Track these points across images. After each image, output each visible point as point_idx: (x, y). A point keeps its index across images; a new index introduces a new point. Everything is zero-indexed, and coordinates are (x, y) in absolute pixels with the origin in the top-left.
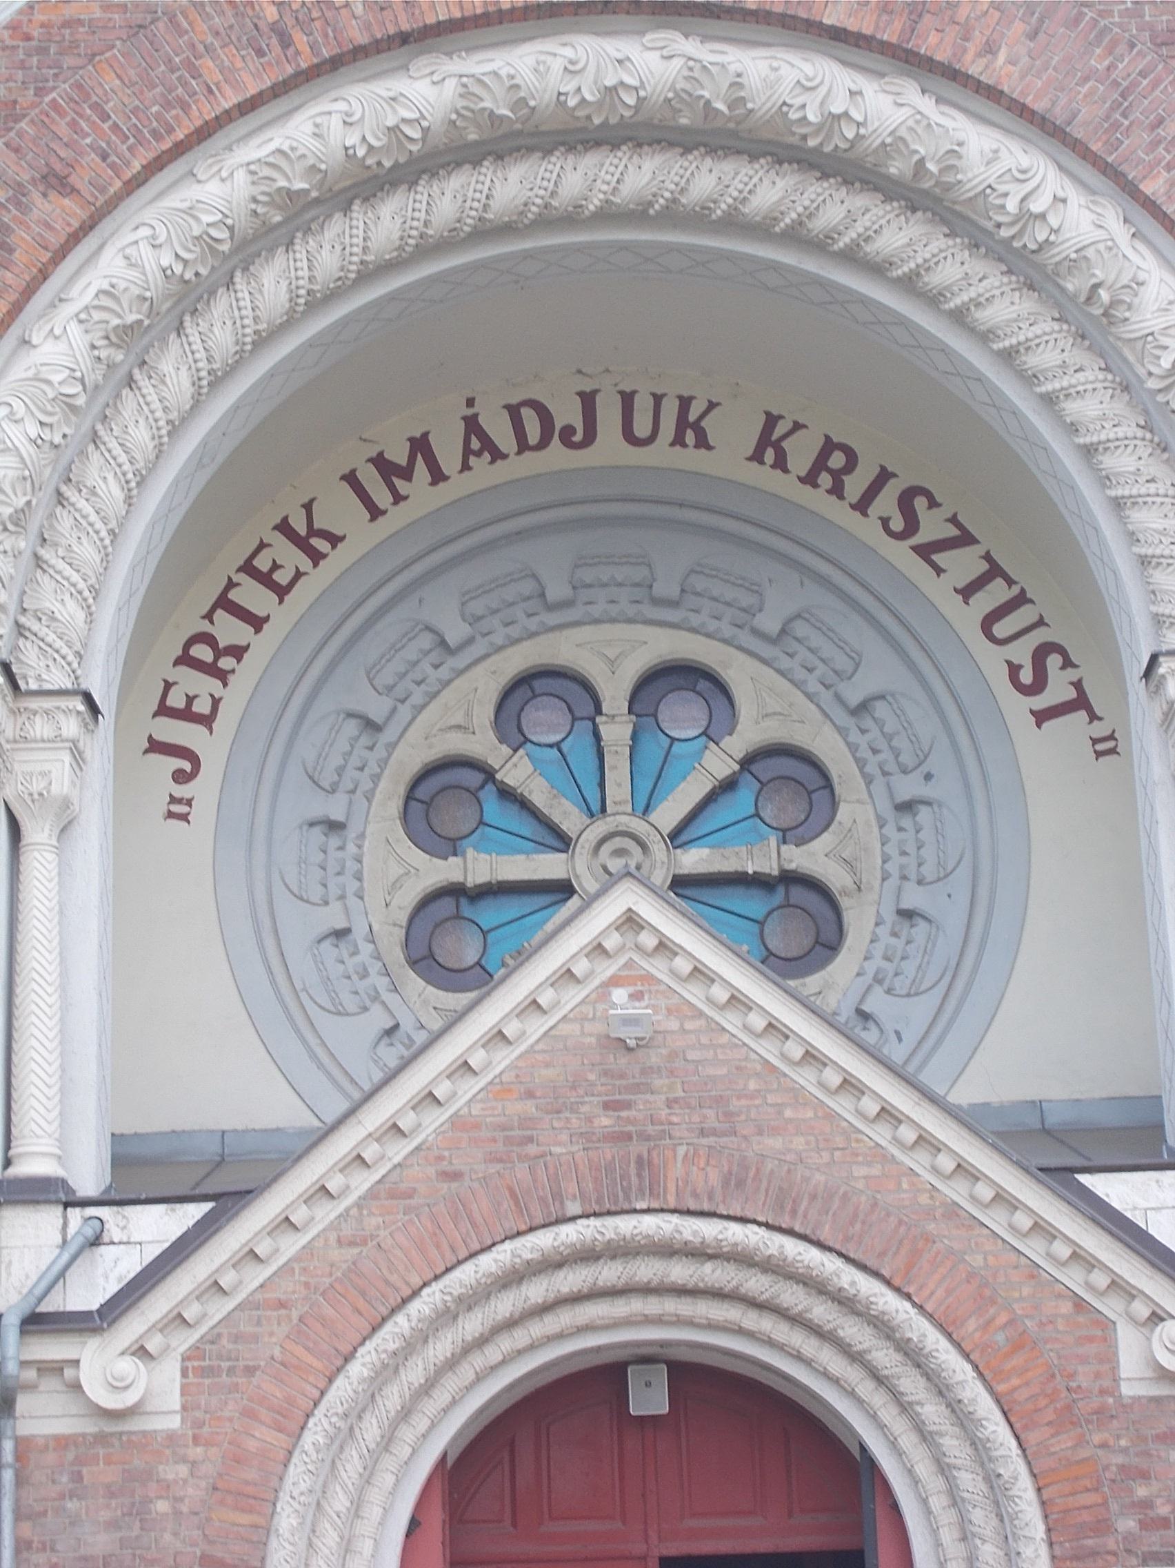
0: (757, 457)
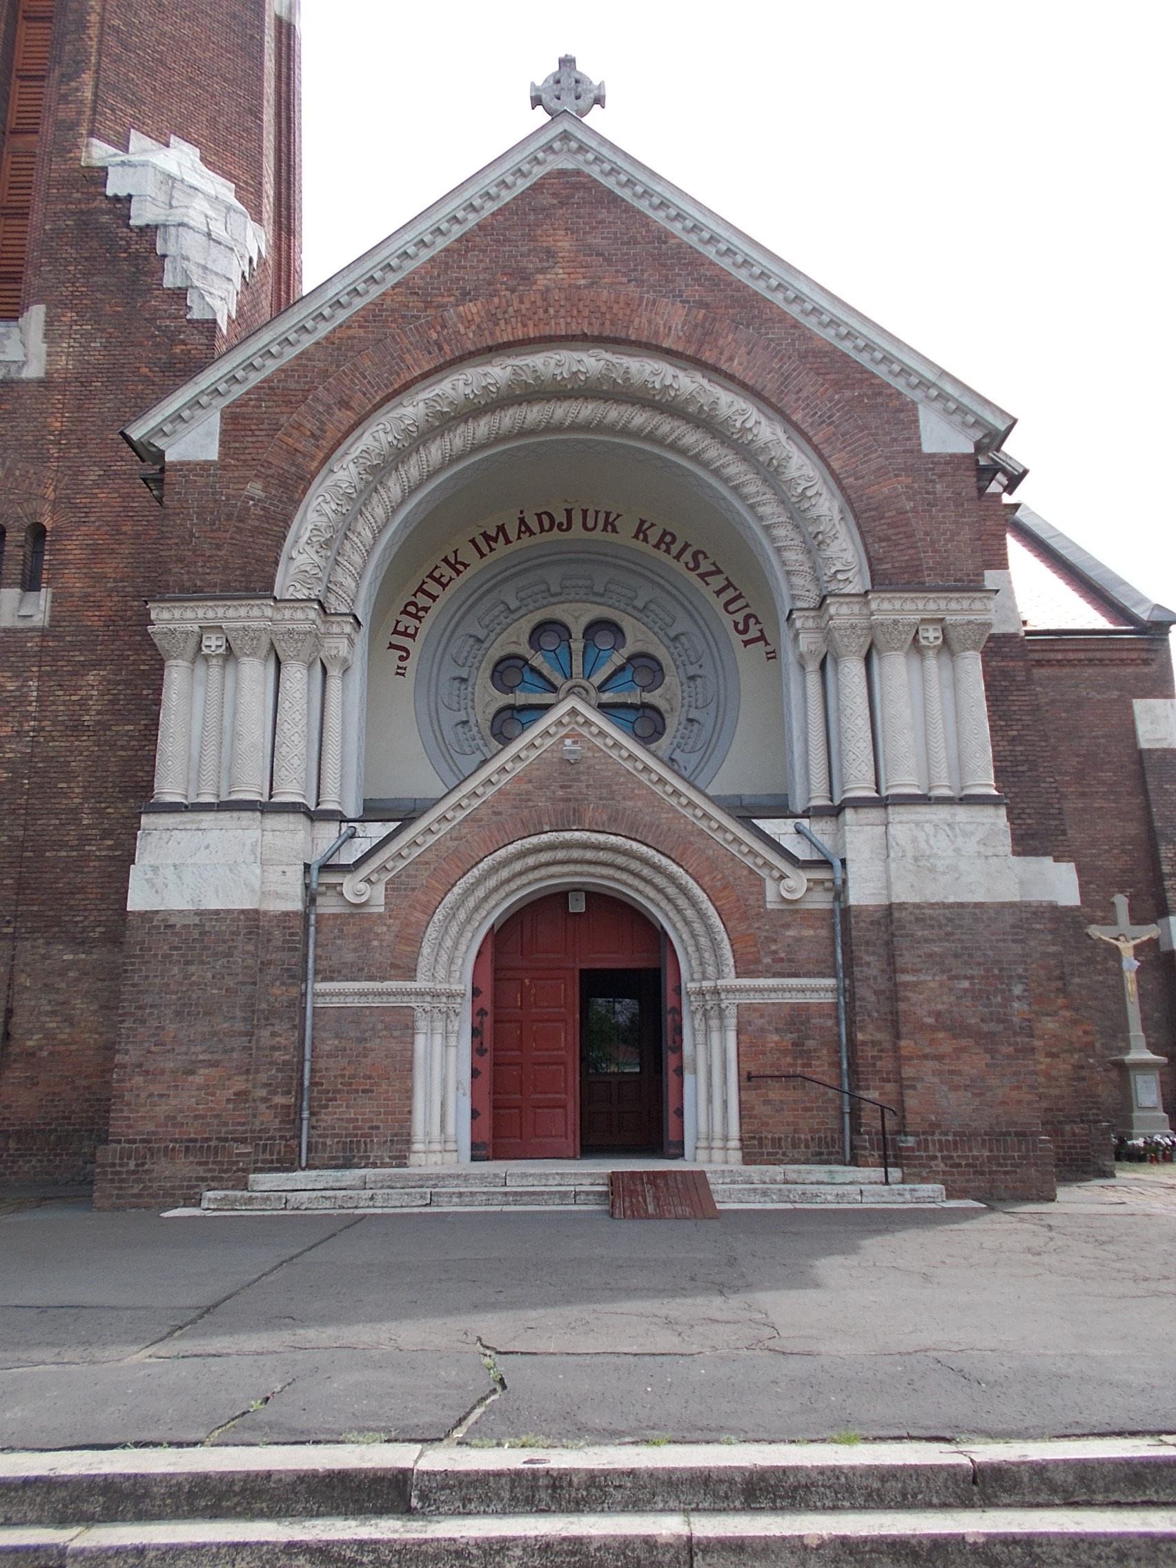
0: (636, 537)
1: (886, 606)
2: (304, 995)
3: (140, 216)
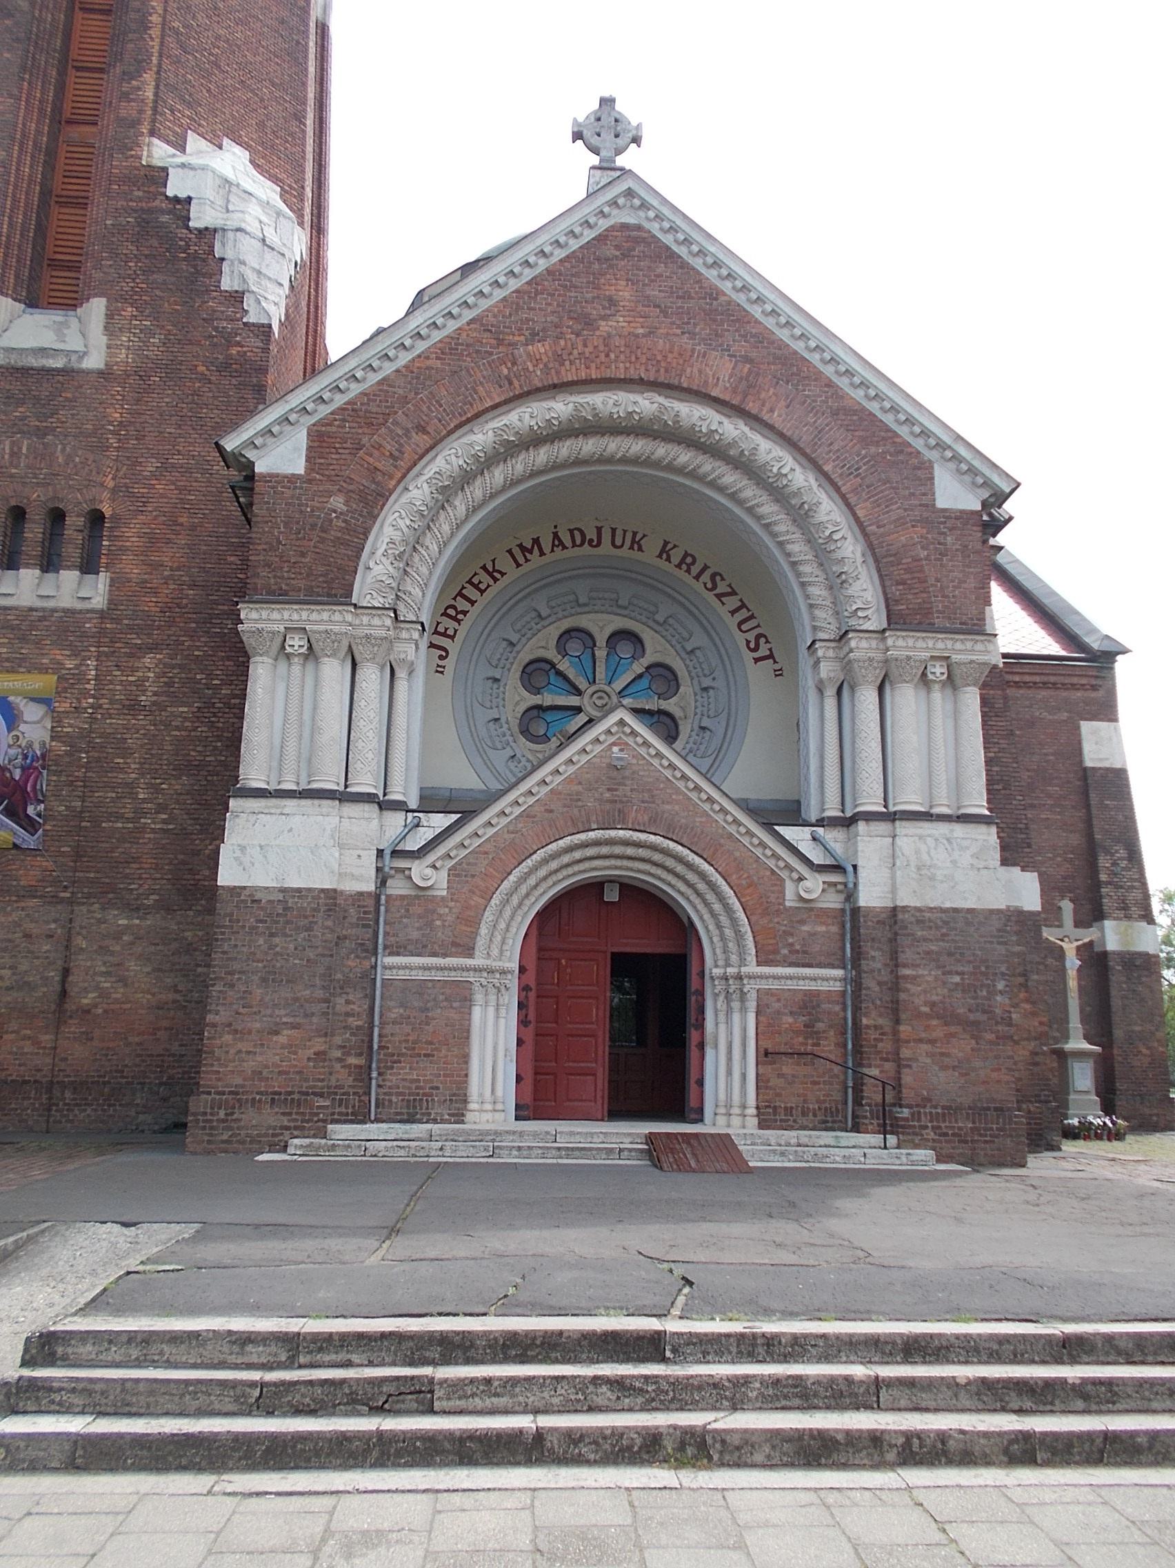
0: (660, 556)
1: (900, 643)
2: (375, 967)
3: (199, 218)
